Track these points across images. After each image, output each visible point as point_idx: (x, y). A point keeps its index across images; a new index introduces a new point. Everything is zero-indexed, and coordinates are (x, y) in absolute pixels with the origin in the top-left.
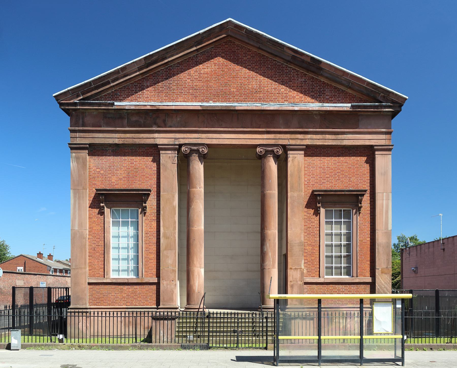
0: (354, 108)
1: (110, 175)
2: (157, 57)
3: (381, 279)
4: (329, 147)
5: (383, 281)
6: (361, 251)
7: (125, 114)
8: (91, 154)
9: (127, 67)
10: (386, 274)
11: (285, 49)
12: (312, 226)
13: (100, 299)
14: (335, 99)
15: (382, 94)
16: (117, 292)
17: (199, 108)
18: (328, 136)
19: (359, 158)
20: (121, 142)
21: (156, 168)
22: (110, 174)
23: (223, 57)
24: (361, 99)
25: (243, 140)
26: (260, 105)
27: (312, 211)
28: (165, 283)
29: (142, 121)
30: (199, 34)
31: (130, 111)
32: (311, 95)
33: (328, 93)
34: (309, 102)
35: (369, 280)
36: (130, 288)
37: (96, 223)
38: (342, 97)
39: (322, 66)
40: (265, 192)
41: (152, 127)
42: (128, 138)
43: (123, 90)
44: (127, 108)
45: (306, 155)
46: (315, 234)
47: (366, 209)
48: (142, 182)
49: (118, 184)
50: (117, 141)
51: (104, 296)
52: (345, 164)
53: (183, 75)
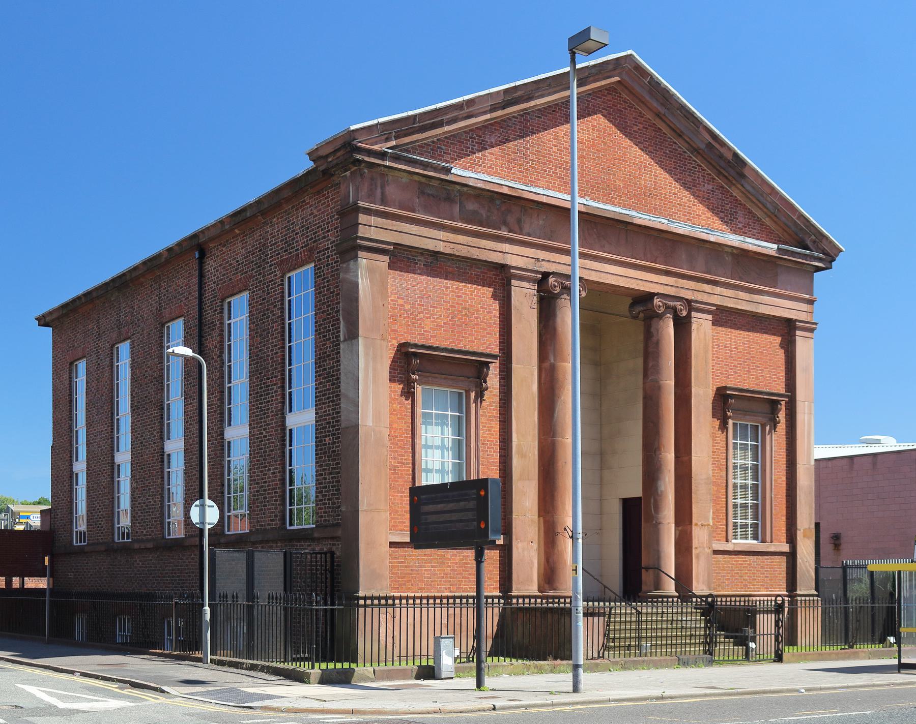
0: (781, 252)
2: (523, 92)
4: (737, 313)
7: (456, 192)
9: (477, 100)
11: (701, 129)
13: (404, 577)
15: (813, 237)
16: (435, 563)
20: (448, 251)
21: (498, 312)
22: (422, 313)
24: (780, 238)
25: (634, 280)
26: (667, 221)
27: (399, 387)
28: (520, 545)
29: (483, 212)
33: (741, 218)
34: (717, 229)
35: (786, 548)
36: (456, 556)
37: (397, 415)
39: (746, 172)
40: (661, 382)
41: (499, 229)
42: (460, 244)
43: (451, 143)
44: (470, 184)
45: (715, 323)
48: (476, 339)
49: (435, 337)
50: (441, 247)
51: (412, 570)
53: (546, 136)
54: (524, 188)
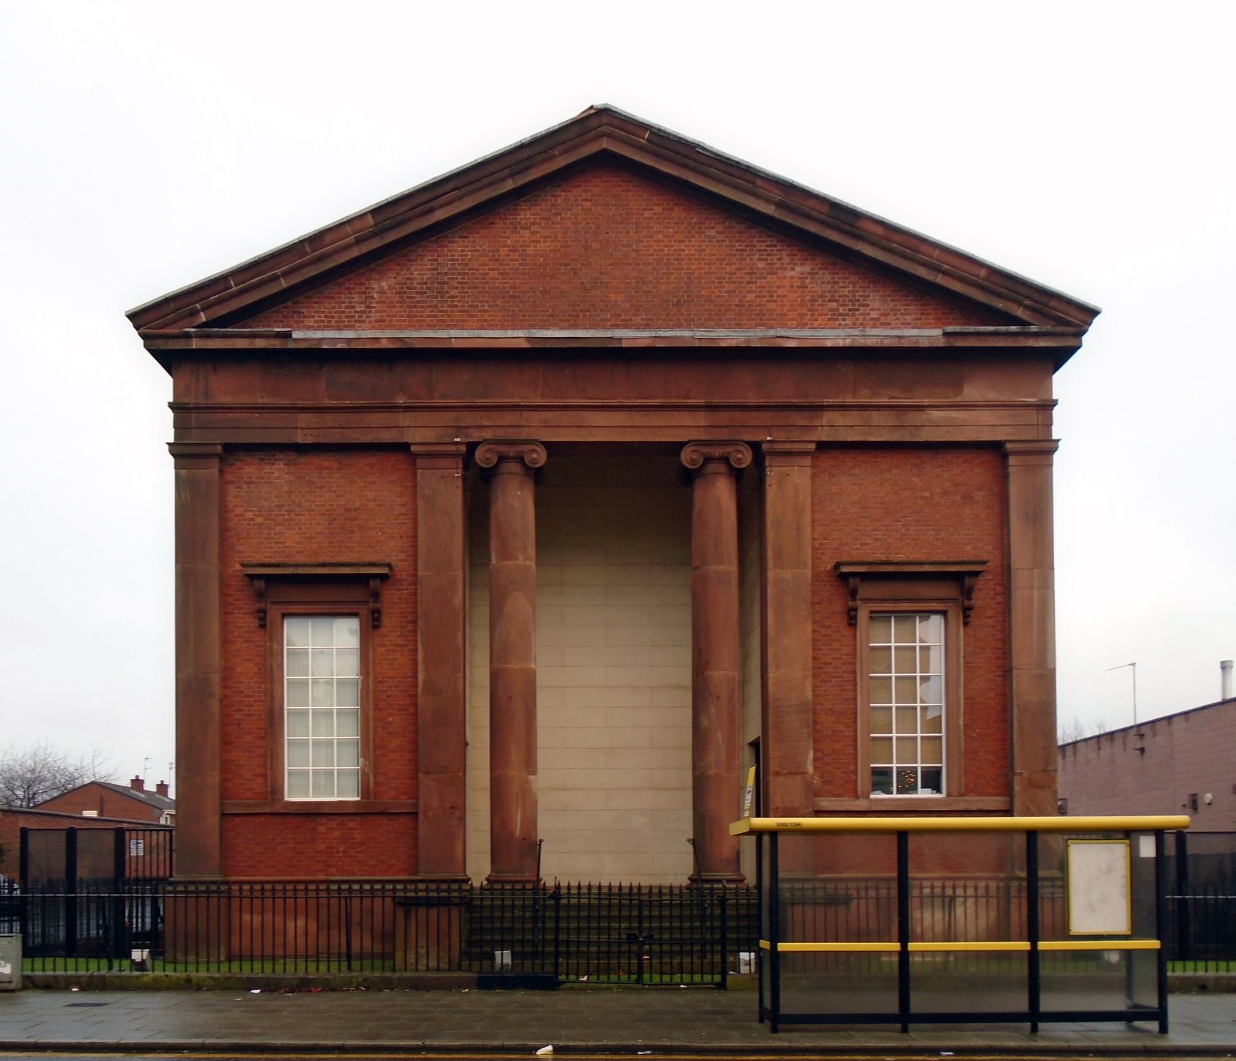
17: (733, 343)
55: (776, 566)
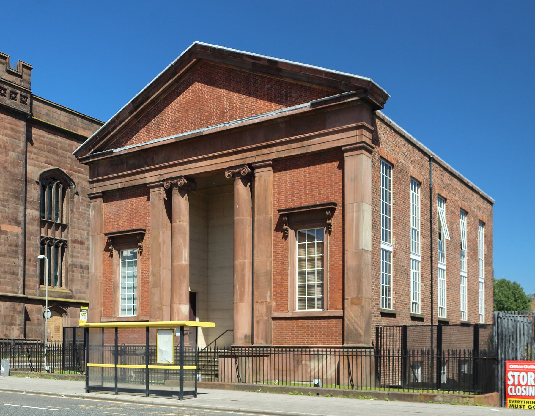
1: (118, 219)
3: (350, 312)
5: (353, 314)
6: (332, 277)
8: (105, 201)
10: (356, 304)
11: (244, 58)
12: (281, 251)
14: (301, 100)
17: (174, 141)
18: (294, 145)
19: (330, 164)
23: (198, 82)
26: (224, 125)
27: (281, 234)
30: (172, 66)
31: (127, 155)
32: (277, 102)
38: (309, 96)
39: (279, 66)
41: (143, 167)
45: (274, 171)
46: (284, 261)
47: (338, 225)
50: (120, 186)
52: (316, 175)
54: (145, 144)
55: (28, 240)
